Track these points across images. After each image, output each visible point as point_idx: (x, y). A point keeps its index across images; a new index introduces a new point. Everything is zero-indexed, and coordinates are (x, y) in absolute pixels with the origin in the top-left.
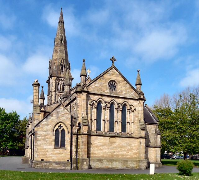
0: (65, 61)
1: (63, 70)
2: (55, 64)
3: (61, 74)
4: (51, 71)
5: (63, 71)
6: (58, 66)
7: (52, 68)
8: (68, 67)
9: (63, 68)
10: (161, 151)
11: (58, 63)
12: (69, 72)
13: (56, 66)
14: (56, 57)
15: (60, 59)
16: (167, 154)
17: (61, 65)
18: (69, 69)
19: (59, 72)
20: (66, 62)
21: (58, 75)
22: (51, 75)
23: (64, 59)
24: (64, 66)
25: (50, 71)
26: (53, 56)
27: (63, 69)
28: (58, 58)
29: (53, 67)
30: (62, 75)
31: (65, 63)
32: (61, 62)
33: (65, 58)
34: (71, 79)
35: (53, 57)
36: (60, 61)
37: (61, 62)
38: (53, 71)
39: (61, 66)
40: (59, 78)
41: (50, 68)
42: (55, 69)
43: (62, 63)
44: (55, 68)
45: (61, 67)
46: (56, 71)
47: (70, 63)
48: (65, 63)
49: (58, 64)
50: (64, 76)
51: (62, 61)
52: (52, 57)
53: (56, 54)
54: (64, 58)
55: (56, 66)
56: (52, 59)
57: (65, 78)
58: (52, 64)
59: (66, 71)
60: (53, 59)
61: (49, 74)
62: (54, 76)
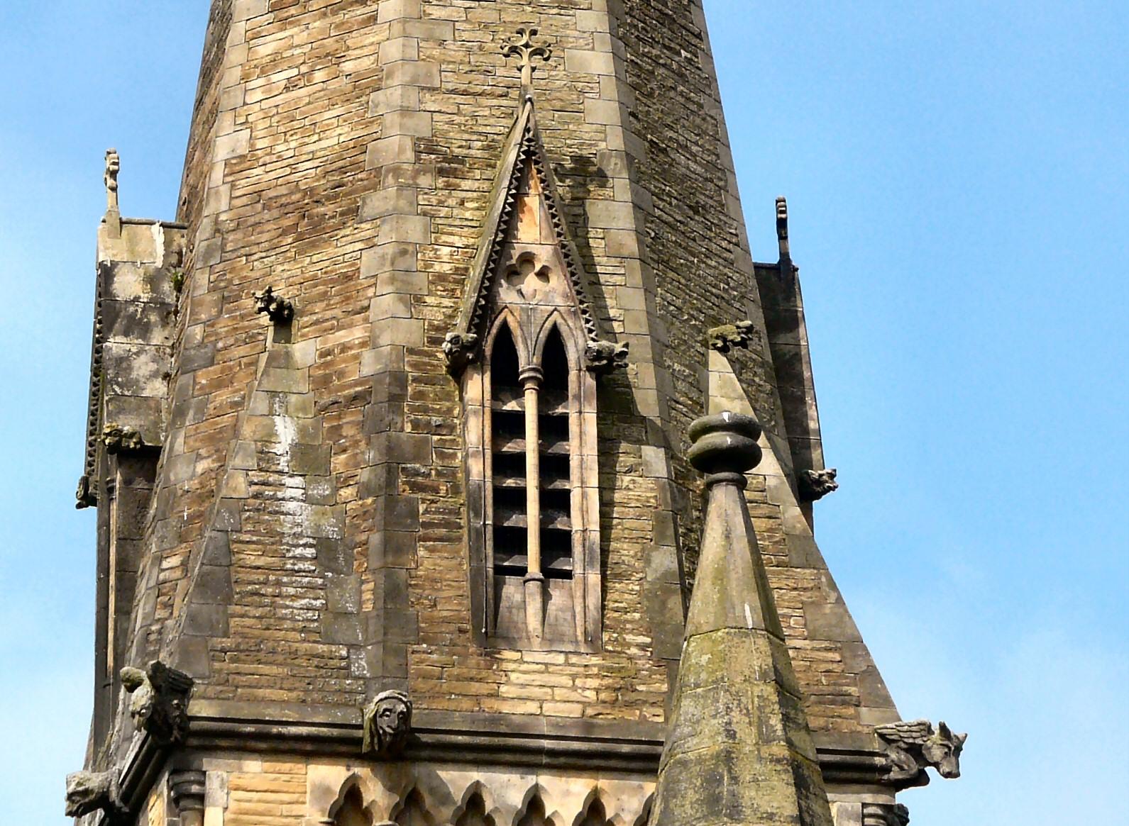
0: (614, 216)
1: (555, 502)
2: (304, 350)
3: (491, 631)
4: (164, 565)
5: (583, 518)
6: (395, 388)
7: (184, 468)
8: (726, 394)
9: (554, 428)
10: (901, 789)
11: (385, 303)
12: (783, 559)
13: (333, 401)
14: (337, 136)
15: (452, 169)
16: (421, 520)
17: (485, 348)
18: (769, 468)
19: (443, 571)
20: (657, 256)
21: (395, 668)
22: (171, 686)
23: (586, 172)
24: (607, 370)
25: (118, 580)
26: (206, 113)
27: (555, 466)
28: (395, 146)
29: (220, 442)
30: (543, 684)
31: (626, 300)
32: (504, 263)
33: (634, 119)
34: (852, 770)
35: (228, 142)
36: (459, 245)
37: (504, 263)
38: (218, 582)
39: (506, 380)
40: (457, 780)
41: (124, 466)
42: (268, 452)
43: (537, 300)
44: (309, 459)
45: (507, 426)
46: (326, 551)
47: (779, 283)
48: (626, 300)
49: (383, 332)
50: (622, 690)
51: (533, 233)
52: (200, 145)
53: (300, 36)
54: (600, 126)
55: (333, 401)
56: (191, 203)
57: (642, 761)
58: (178, 367)
59: (682, 524)
60: (219, 204)
61: (108, 683)
62: (277, 703)
